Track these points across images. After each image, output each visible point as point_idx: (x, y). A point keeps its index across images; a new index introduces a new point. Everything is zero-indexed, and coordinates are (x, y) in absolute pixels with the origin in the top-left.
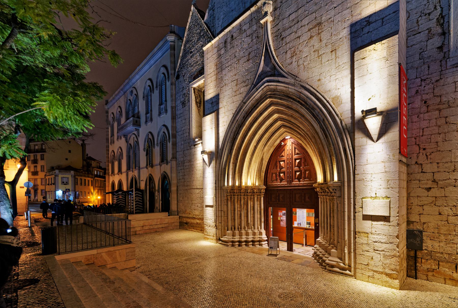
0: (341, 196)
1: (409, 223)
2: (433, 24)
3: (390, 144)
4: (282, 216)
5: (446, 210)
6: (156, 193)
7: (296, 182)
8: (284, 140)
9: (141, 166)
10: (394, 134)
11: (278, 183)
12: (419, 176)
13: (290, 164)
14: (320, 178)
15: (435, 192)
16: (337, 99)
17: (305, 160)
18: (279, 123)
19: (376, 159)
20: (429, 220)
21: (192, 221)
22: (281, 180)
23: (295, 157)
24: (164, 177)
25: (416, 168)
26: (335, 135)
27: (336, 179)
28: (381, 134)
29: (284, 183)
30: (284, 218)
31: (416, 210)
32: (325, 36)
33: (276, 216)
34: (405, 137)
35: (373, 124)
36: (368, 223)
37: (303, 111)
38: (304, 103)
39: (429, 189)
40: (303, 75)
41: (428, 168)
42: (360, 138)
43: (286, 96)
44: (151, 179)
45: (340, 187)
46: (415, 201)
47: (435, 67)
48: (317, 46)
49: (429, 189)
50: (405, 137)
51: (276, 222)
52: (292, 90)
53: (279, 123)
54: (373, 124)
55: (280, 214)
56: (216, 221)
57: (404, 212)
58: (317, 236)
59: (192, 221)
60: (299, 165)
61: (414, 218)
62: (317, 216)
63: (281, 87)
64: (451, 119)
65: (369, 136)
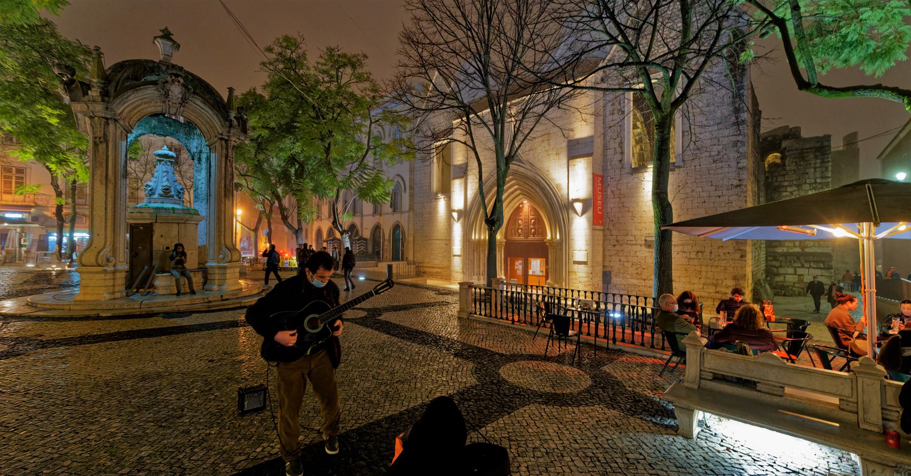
0: (561, 249)
1: (604, 266)
2: (617, 145)
3: (588, 219)
4: (519, 266)
5: (623, 259)
6: (386, 243)
7: (531, 238)
8: (522, 203)
9: (364, 213)
10: (590, 213)
11: (517, 238)
12: (609, 237)
13: (527, 223)
14: (549, 237)
15: (617, 247)
16: (558, 186)
17: (539, 220)
18: (518, 192)
19: (580, 227)
20: (615, 265)
21: (432, 270)
22: (519, 235)
23: (531, 217)
24: (397, 227)
25: (608, 232)
26: (557, 209)
27: (558, 237)
28: (583, 213)
29: (522, 238)
30: (520, 267)
31: (608, 258)
32: (552, 142)
33: (513, 265)
34: (308, 353)
35: (578, 206)
36: (576, 266)
37: (538, 189)
38: (538, 184)
39: (614, 246)
40: (538, 165)
41: (614, 233)
42: (571, 212)
43: (526, 177)
44: (377, 228)
45: (560, 243)
46: (607, 253)
47: (618, 172)
48: (547, 148)
49: (614, 246)
50: (308, 353)
51: (513, 271)
52: (529, 173)
53: (518, 192)
54: (578, 206)
55: (517, 263)
56: (463, 268)
57: (600, 258)
58: (547, 279)
59: (432, 270)
60: (534, 224)
61: (607, 264)
62: (547, 264)
63: (521, 170)
64: (625, 204)
65: (577, 213)
